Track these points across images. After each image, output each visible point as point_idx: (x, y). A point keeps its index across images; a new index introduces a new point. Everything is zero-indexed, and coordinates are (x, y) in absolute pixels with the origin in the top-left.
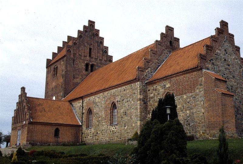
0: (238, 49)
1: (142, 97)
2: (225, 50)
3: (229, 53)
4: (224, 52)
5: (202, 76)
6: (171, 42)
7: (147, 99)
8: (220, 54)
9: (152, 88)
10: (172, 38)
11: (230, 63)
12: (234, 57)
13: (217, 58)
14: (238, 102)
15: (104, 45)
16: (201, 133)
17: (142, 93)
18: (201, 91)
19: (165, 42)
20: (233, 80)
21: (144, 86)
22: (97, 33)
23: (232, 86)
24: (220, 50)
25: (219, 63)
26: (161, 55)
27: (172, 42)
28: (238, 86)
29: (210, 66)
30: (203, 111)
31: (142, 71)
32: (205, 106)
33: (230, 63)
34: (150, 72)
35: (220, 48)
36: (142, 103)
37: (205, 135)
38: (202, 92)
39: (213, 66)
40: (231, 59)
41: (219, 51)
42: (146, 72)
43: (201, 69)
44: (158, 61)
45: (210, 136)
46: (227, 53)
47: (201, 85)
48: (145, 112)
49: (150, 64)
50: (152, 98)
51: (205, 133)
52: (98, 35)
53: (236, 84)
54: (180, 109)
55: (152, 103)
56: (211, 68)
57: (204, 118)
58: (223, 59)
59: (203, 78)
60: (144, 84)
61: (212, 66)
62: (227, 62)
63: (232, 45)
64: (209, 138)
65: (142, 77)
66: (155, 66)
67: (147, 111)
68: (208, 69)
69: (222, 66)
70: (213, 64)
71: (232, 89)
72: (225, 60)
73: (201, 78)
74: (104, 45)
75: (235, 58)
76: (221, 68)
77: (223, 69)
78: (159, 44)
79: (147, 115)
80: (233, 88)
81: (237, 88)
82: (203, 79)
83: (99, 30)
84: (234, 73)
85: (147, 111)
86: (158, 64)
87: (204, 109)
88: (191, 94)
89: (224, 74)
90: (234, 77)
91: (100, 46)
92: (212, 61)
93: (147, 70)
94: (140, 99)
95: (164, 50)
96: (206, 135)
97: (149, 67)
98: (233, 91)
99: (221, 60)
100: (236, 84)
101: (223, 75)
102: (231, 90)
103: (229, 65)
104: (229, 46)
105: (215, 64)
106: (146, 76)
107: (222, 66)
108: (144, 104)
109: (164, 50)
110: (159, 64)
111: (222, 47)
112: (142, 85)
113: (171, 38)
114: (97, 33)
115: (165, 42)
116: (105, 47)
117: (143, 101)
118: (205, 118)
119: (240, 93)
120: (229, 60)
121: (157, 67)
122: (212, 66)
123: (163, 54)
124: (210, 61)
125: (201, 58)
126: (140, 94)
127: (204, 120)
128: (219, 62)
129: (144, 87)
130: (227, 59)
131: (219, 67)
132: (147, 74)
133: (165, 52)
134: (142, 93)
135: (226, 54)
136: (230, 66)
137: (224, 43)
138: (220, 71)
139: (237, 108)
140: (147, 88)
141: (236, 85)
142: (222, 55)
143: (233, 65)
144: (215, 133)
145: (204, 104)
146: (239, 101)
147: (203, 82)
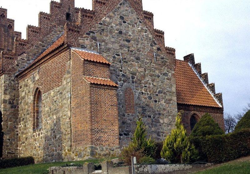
0: (149, 16)
1: (8, 97)
2: (122, 18)
3: (129, 22)
4: (119, 21)
5: (70, 58)
6: (68, 15)
7: (18, 100)
8: (109, 23)
9: (24, 83)
10: (71, 9)
11: (132, 37)
12: (140, 28)
13: (103, 30)
14: (146, 98)
15: (15, 30)
16: (67, 150)
17: (8, 92)
18: (68, 83)
19: (57, 15)
20: (137, 64)
21: (13, 81)
22: (3, 14)
23: (134, 74)
24: (110, 17)
25: (108, 38)
26: (48, 34)
27: (70, 14)
28: (147, 72)
29: (87, 42)
30: (69, 113)
31: (11, 58)
32: (72, 107)
33: (132, 37)
34: (26, 59)
35: (111, 14)
36: (8, 106)
37: (70, 154)
38: (69, 84)
39: (94, 41)
40: (134, 31)
41: (108, 19)
42: (19, 59)
43: (69, 47)
44: (43, 42)
45: (76, 156)
46: (125, 22)
47: (69, 73)
48: (14, 120)
49: (26, 47)
50: (24, 98)
51: (70, 151)
52: (4, 16)
53: (142, 69)
54: (48, 113)
55: (23, 106)
56: (88, 46)
57: (70, 127)
58: (117, 32)
59: (71, 61)
60: (13, 78)
61: (91, 43)
62: (124, 36)
63: (136, 9)
64: (74, 159)
65: (10, 66)
66: (37, 50)
67: (17, 118)
68: (83, 47)
69: (113, 43)
70: (94, 38)
71: (133, 78)
72: (121, 33)
73: (69, 62)
74: (15, 30)
75: (142, 29)
76: (110, 46)
77: (116, 46)
78: (44, 18)
79: (18, 125)
80: (135, 77)
81: (144, 76)
82: (71, 63)
83: (6, 10)
84: (138, 53)
85: (17, 118)
86: (42, 48)
87: (71, 111)
88: (58, 88)
89: (119, 55)
90: (138, 59)
91: (8, 31)
92: (91, 34)
93: (20, 57)
94: (5, 101)
95: (55, 26)
96: (72, 153)
97: (24, 53)
98: (134, 80)
99: (111, 32)
100: (142, 69)
101: (116, 56)
102: (131, 79)
103: (128, 41)
104: (130, 10)
105: (97, 38)
106: (18, 65)
107: (113, 43)
108: (12, 107)
109: (55, 26)
110: (44, 48)
111: (116, 13)
112: (9, 79)
113: (69, 9)
114: (3, 14)
115: (57, 15)
116: (16, 32)
117: (10, 103)
118: (71, 126)
119: (150, 84)
120: (130, 33)
121: (40, 51)
122: (91, 43)
123: (53, 33)
124: (88, 34)
125: (70, 30)
126: (5, 94)
127: (70, 129)
128: (107, 36)
129: (12, 82)
130: (124, 32)
131: (106, 44)
132: (20, 62)
133: (57, 29)
134: (8, 92)
135: (123, 23)
136: (132, 42)
137: (119, 6)
138: (109, 50)
139: (143, 107)
140: (18, 84)
141: (143, 71)
142: (113, 25)
143: (137, 41)
144: (81, 150)
145: (71, 103)
146: (147, 96)
147: (71, 67)
